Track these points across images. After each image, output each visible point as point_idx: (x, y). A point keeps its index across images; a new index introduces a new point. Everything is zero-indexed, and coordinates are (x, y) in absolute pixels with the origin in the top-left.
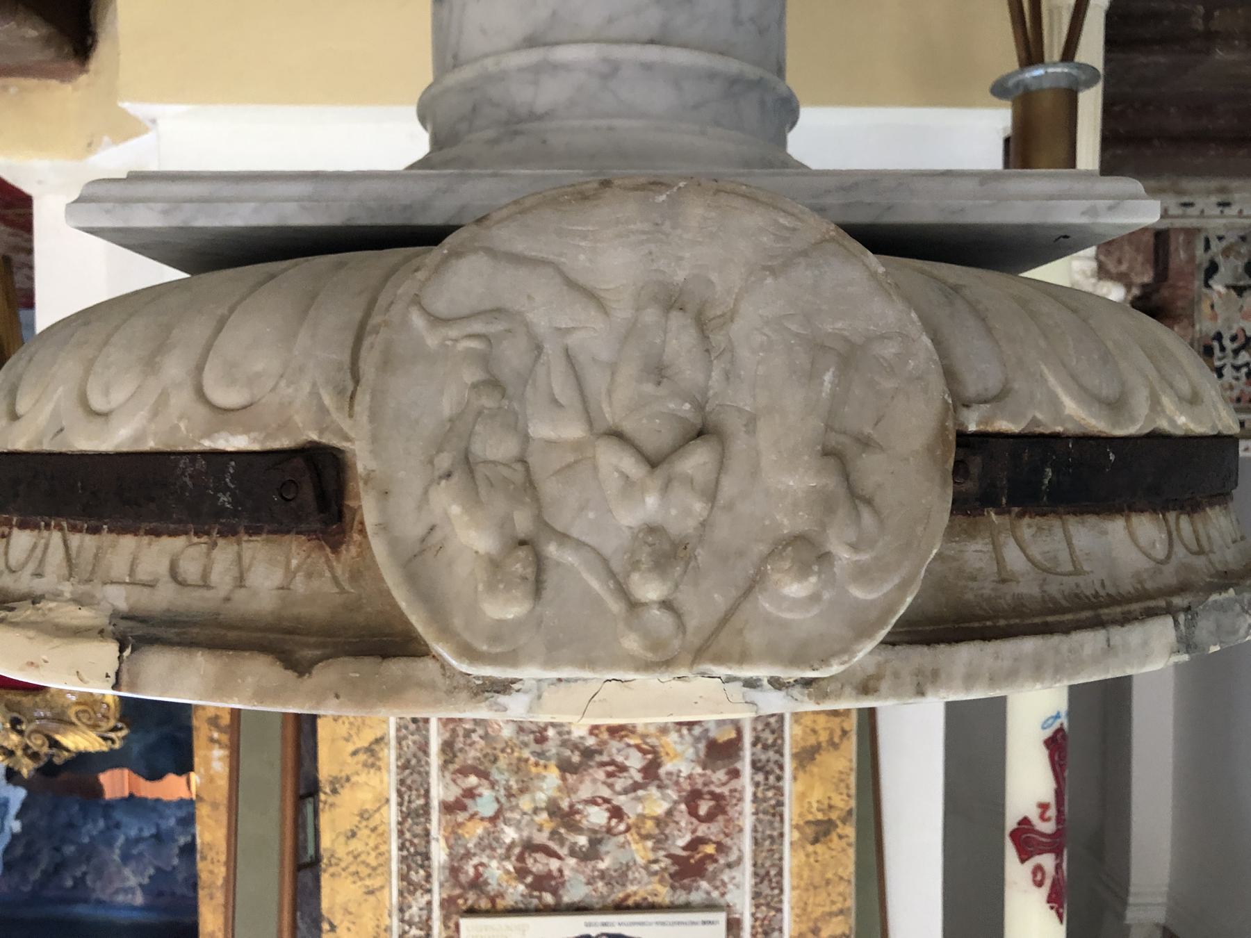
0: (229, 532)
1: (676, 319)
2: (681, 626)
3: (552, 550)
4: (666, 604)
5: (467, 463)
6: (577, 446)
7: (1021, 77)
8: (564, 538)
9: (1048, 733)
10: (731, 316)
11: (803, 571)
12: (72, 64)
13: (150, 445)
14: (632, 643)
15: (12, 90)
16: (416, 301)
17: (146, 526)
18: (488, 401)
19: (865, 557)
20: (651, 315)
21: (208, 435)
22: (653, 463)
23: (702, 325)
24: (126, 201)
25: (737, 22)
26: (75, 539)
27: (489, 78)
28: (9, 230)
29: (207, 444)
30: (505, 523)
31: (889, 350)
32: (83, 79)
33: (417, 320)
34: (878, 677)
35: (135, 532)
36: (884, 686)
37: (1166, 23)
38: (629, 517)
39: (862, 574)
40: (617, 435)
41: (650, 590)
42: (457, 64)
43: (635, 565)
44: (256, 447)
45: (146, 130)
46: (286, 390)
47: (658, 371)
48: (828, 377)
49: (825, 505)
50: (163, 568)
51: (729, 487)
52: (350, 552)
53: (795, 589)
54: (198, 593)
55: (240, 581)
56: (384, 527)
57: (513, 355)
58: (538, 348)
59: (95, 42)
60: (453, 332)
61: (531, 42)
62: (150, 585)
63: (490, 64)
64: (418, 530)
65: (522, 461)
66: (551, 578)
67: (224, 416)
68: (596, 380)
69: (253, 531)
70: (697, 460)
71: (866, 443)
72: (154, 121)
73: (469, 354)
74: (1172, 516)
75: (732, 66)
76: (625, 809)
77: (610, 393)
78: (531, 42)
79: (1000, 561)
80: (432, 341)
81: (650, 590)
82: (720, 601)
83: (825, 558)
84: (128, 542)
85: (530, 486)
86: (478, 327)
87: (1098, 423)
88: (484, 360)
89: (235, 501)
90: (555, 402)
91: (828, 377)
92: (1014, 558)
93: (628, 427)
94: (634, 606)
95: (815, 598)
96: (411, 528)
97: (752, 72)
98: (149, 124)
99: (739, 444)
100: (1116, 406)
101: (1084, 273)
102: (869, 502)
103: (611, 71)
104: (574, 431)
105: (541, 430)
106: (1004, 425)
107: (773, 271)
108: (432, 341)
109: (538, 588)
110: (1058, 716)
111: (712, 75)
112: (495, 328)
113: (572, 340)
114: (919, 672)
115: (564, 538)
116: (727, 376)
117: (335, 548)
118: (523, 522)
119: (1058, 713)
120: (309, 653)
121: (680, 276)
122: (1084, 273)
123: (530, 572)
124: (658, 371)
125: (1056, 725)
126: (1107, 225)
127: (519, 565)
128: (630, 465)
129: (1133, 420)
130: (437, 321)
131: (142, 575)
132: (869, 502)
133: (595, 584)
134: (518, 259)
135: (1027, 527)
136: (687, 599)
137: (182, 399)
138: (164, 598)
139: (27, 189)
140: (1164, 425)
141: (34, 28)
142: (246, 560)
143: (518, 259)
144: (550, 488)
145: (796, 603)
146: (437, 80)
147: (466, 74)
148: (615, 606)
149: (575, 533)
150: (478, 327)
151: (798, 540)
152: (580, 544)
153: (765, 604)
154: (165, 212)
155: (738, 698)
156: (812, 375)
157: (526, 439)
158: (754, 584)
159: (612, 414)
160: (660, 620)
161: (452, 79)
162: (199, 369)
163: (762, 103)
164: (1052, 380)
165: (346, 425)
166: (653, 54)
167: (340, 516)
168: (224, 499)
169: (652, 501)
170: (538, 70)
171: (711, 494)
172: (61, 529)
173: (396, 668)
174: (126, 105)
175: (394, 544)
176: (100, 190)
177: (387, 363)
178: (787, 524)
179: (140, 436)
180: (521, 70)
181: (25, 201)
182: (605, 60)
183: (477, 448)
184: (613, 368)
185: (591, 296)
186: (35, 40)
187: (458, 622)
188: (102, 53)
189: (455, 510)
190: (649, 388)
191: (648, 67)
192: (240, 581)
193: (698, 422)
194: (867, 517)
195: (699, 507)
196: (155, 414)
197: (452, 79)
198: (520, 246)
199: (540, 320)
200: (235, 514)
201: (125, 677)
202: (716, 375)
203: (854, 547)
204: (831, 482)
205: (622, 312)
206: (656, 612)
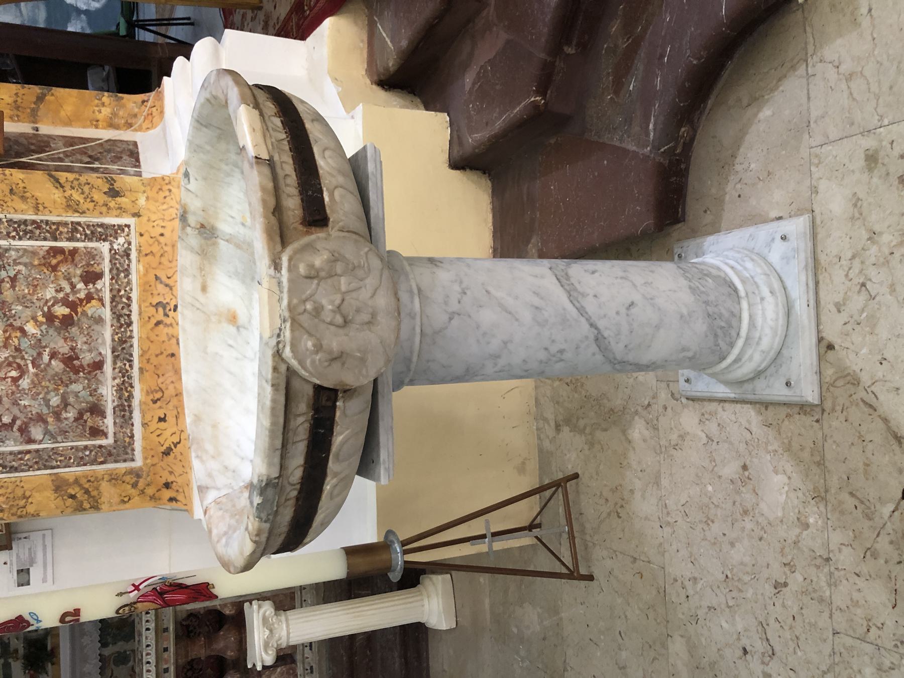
0: (301, 193)
1: (370, 316)
2: (299, 314)
3: (315, 281)
4: (305, 310)
5: (336, 260)
6: (339, 289)
7: (396, 542)
8: (318, 284)
9: (27, 617)
10: (370, 330)
11: (314, 346)
12: (376, 78)
13: (321, 172)
14: (295, 301)
15: (361, 45)
16: (371, 250)
17: (297, 167)
18: (350, 266)
19: (317, 362)
20: (371, 310)
21: (327, 189)
22: (339, 307)
23: (369, 323)
24: (375, 161)
25: (428, 361)
26: (286, 143)
27: (407, 275)
28: (282, 18)
29: (325, 189)
30: (322, 269)
31: (364, 372)
32: (368, 82)
33: (366, 249)
34: (278, 373)
35: (294, 164)
36: (276, 374)
37: (416, 664)
38: (324, 302)
39: (313, 362)
40: (343, 300)
41: (309, 306)
42: (410, 265)
43: (314, 302)
44: (326, 203)
45: (348, 112)
46: (341, 212)
47: (358, 311)
48: (359, 354)
49: (331, 352)
50: (287, 172)
51: (332, 328)
52: (301, 227)
53: (310, 344)
54: (283, 183)
55: (289, 196)
56: (318, 238)
57: (360, 273)
58: (361, 280)
59: (386, 90)
60: (364, 258)
61: (419, 290)
62: (282, 169)
63: (411, 276)
64: (318, 247)
65: (336, 275)
66: (308, 281)
67: (331, 195)
68: (354, 295)
69: (302, 200)
70: (339, 320)
71: (343, 364)
72: (353, 117)
73: (360, 262)
74: (298, 487)
75: (415, 359)
76: (159, 319)
77: (352, 298)
78: (419, 290)
79: (299, 415)
80: (362, 253)
81: (309, 306)
82: (306, 325)
83: (317, 352)
84: (291, 161)
85: (331, 276)
86: (366, 265)
87: (334, 449)
88: (359, 266)
89: (310, 196)
90: (350, 284)
91: (359, 354)
92: (301, 420)
93: (345, 302)
94: (305, 301)
95: (307, 350)
96: (319, 245)
97: (413, 367)
98: (351, 114)
99: (341, 331)
100: (337, 456)
101: (280, 639)
102: (330, 365)
103: (412, 316)
104: (343, 288)
105: (343, 280)
106: (338, 414)
107: (381, 342)
108: (362, 253)
109: (308, 277)
110: (38, 621)
111: (412, 352)
112: (366, 269)
113: (363, 289)
114: (278, 385)
115: (318, 284)
116: (357, 329)
117: (301, 224)
118: (323, 274)
119: (41, 621)
120: (277, 215)
121: (379, 318)
122: (280, 639)
123: (312, 275)
124: (358, 311)
125: (32, 621)
126: (379, 473)
127: (313, 273)
128: (338, 302)
129: (333, 463)
130: (366, 254)
131: (284, 165)
132: (330, 365)
133: (308, 292)
134: (381, 276)
135: (307, 425)
136: (306, 316)
137: (334, 182)
138: (281, 173)
139: (308, 39)
140: (328, 479)
141: (393, 65)
142: (294, 197)
143: (381, 276)
144: (329, 281)
145: (306, 345)
146: (404, 257)
147: (408, 268)
148: (304, 297)
149: (320, 288)
150: (366, 265)
151: (321, 346)
152: (317, 289)
153: (305, 337)
154: (373, 173)
155: (274, 332)
156: (359, 351)
157: (341, 276)
158: (310, 335)
159: (347, 298)
160: (301, 309)
161: (405, 263)
162: (341, 187)
163: (402, 373)
164: (347, 432)
165: (336, 228)
166: (418, 330)
167: (310, 225)
168: (310, 193)
169: (330, 307)
170: (411, 292)
171: (331, 324)
172: (287, 137)
173: (278, 239)
174: (361, 104)
175: (314, 241)
176: (378, 153)
177: (356, 241)
178: (325, 343)
179: (322, 169)
180: (411, 286)
181: (302, 34)
182: (415, 314)
183: (339, 263)
184: (357, 299)
185: (372, 297)
186: (388, 64)
187: (298, 256)
188: (381, 94)
189: (325, 257)
190: (355, 308)
191: (414, 329)
192: (289, 196)
193: (347, 321)
194: (326, 364)
195: (328, 320)
196: (329, 173)
197: (405, 263)
198: (384, 277)
199: (368, 281)
200: (307, 195)
201: (260, 160)
202: (358, 326)
203: (320, 360)
204: (335, 355)
205: (370, 303)
206: (303, 308)
